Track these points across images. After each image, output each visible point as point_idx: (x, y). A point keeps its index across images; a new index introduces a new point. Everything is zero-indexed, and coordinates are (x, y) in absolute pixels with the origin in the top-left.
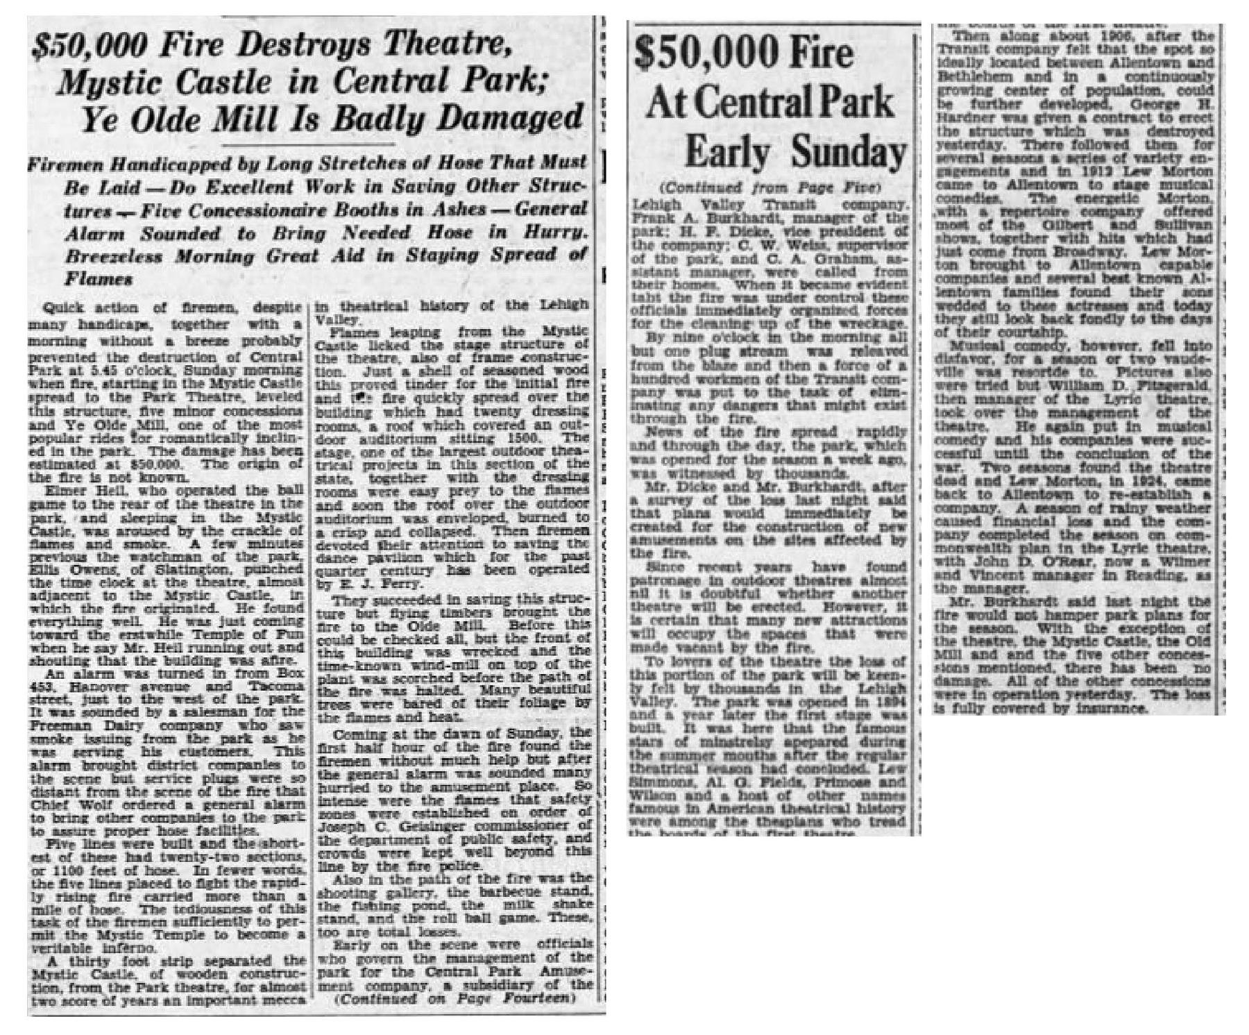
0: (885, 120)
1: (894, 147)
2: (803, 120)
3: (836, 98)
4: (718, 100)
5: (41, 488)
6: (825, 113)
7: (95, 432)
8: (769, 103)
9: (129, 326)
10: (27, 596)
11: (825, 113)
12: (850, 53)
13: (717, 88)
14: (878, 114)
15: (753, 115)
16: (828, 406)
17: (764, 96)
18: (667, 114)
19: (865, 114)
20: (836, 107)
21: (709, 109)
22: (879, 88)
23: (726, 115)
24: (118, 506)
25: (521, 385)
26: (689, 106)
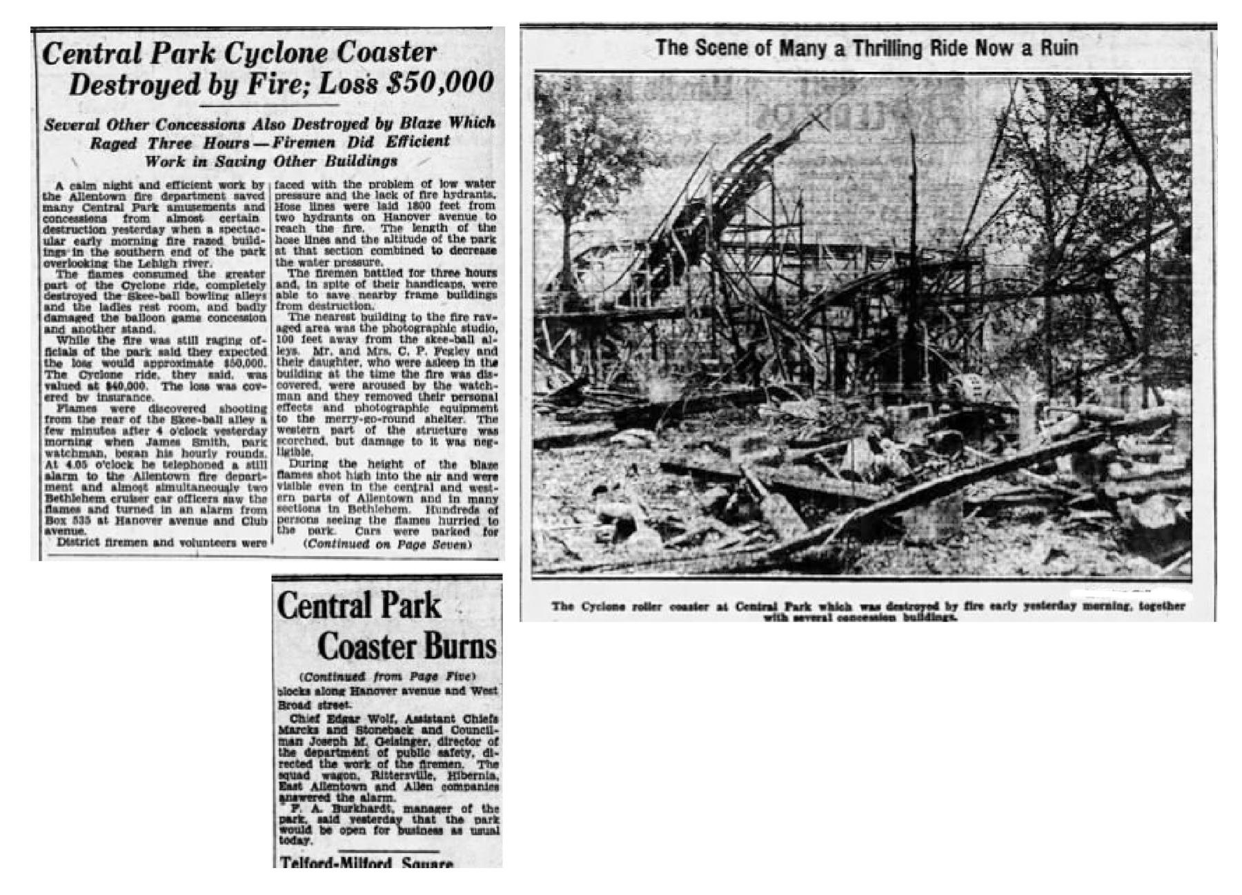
3: (394, 603)
4: (296, 604)
6: (386, 614)
8: (337, 606)
11: (386, 614)
14: (428, 616)
15: (324, 616)
19: (418, 615)
20: (394, 610)
25: (177, 352)
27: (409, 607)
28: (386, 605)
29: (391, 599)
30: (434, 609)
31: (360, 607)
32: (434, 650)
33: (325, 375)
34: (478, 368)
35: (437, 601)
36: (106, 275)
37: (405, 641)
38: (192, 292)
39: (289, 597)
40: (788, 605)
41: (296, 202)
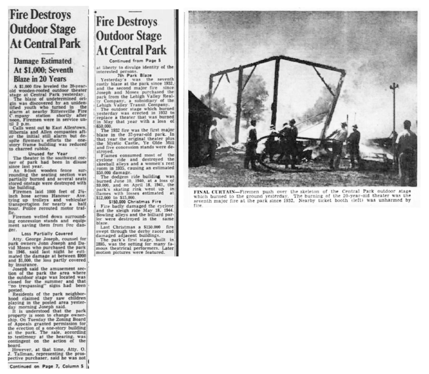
0: (78, 49)
1: (149, 20)
2: (140, 55)
5: (12, 191)
6: (61, 47)
8: (45, 44)
9: (124, 173)
11: (61, 47)
12: (75, 29)
13: (116, 46)
14: (76, 47)
17: (130, 48)
18: (16, 47)
19: (158, 53)
20: (64, 45)
21: (28, 46)
22: (162, 46)
23: (33, 47)
26: (108, 51)
27: (155, 51)
28: (147, 50)
30: (78, 45)
31: (53, 44)
33: (39, 159)
34: (15, 330)
36: (59, 99)
37: (122, 48)
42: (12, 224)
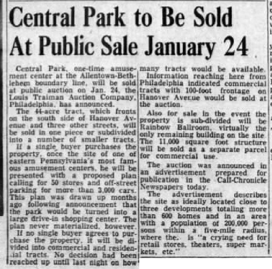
0: (120, 27)
3: (93, 15)
4: (22, 16)
7: (166, 241)
10: (11, 266)
13: (21, 10)
14: (116, 25)
16: (252, 245)
17: (48, 14)
18: (21, 53)
20: (93, 21)
21: (17, 22)
24: (30, 248)
27: (103, 18)
29: (90, 13)
32: (168, 21)
35: (122, 14)
37: (33, 14)
38: (189, 139)
39: (17, 12)
40: (51, 68)
41: (197, 213)
42: (60, 259)
